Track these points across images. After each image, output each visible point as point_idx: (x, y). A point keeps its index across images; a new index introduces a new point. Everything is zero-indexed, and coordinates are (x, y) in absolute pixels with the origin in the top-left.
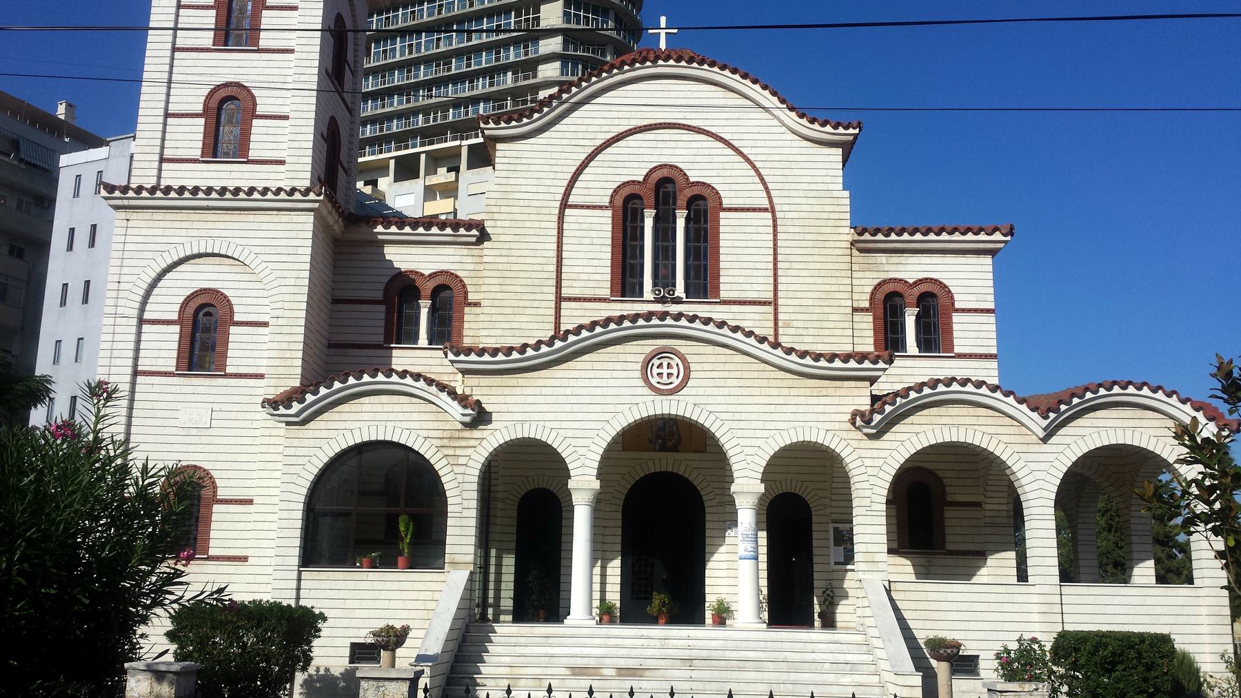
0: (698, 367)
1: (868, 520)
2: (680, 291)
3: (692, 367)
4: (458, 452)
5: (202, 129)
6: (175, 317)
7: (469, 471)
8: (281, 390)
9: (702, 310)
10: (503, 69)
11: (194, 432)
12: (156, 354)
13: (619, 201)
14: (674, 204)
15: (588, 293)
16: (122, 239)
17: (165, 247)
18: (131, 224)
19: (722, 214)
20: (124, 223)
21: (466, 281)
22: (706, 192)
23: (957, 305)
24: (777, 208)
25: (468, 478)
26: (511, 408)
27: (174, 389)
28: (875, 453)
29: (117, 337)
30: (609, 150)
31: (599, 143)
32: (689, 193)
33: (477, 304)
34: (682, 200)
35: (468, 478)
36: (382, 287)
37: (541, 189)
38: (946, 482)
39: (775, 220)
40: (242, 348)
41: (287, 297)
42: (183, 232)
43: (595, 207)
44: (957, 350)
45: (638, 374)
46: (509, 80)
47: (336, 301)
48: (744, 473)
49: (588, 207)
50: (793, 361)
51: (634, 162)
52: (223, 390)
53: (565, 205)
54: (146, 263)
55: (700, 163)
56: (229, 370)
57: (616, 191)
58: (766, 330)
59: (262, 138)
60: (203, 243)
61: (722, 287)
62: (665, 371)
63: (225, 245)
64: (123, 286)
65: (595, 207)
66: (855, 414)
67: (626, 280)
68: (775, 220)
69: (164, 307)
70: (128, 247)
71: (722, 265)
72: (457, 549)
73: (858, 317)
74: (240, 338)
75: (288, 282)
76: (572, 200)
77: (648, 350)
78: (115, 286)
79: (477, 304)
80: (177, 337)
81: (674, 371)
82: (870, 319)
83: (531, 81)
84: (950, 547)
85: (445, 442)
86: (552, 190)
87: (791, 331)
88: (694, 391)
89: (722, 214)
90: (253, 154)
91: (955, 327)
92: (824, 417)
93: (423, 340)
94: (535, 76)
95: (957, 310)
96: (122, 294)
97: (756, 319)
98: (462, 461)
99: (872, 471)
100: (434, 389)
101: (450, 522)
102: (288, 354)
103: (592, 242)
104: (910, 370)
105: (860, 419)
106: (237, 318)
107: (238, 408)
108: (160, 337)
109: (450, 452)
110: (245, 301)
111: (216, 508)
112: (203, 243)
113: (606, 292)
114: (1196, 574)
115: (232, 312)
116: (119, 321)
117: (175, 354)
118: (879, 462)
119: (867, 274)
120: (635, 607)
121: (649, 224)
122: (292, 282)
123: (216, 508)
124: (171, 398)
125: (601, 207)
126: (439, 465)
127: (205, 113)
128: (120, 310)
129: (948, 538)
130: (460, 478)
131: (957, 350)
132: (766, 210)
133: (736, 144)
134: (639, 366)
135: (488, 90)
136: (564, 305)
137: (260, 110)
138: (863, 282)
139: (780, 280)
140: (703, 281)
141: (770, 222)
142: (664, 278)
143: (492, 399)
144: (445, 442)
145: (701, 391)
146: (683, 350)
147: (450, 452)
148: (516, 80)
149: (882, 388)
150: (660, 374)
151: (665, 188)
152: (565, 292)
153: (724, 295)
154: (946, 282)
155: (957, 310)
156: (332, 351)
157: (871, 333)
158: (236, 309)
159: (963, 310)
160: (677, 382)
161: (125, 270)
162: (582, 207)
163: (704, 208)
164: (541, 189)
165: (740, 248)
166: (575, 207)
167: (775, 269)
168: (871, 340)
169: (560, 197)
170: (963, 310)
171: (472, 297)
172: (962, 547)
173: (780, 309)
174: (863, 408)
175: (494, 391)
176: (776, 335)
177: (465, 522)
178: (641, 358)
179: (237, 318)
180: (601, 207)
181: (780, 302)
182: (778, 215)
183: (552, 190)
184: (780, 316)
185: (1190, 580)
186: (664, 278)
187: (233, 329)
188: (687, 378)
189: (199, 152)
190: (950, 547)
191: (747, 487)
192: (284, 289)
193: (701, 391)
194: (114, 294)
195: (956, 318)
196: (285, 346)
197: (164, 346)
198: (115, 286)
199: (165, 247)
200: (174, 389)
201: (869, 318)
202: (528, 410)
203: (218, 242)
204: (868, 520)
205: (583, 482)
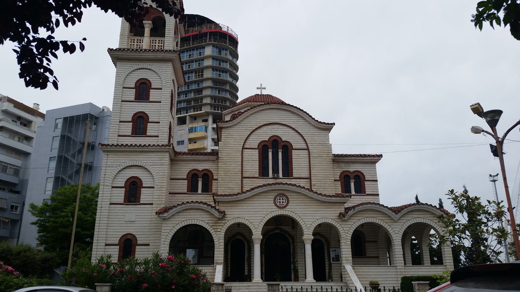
0: (292, 199)
1: (345, 247)
2: (281, 175)
3: (273, 204)
4: (218, 227)
5: (131, 126)
6: (123, 185)
7: (221, 233)
8: (159, 209)
9: (285, 181)
10: (190, 91)
11: (130, 222)
12: (117, 197)
13: (261, 147)
14: (278, 147)
15: (252, 176)
16: (106, 161)
17: (121, 163)
18: (109, 156)
19: (293, 151)
20: (107, 156)
21: (213, 172)
22: (288, 144)
23: (366, 179)
24: (310, 149)
25: (221, 236)
26: (234, 213)
27: (123, 209)
28: (347, 226)
29: (104, 192)
30: (257, 131)
31: (254, 129)
32: (282, 144)
33: (217, 180)
34: (280, 147)
35: (221, 236)
36: (186, 174)
37: (236, 143)
38: (366, 234)
39: (309, 152)
40: (145, 195)
41: (160, 179)
42: (126, 159)
43: (253, 149)
44: (367, 193)
45: (273, 202)
46: (192, 95)
47: (171, 179)
48: (307, 233)
49: (251, 149)
50: (315, 196)
51: (265, 134)
52: (139, 209)
53: (243, 148)
54: (114, 168)
55: (286, 135)
56: (141, 202)
57: (260, 144)
58: (307, 186)
59: (151, 129)
60: (133, 162)
61: (294, 173)
62: (281, 201)
63: (140, 162)
64: (106, 176)
65: (253, 149)
66: (341, 213)
67: (263, 172)
68: (309, 152)
69: (120, 183)
70: (108, 163)
71: (293, 167)
72: (218, 258)
73: (336, 183)
74: (144, 192)
75: (160, 174)
76: (246, 146)
77: (276, 194)
78: (104, 176)
79: (217, 180)
80: (124, 192)
81: (284, 201)
82: (340, 183)
83: (201, 96)
84: (367, 255)
85: (214, 224)
86: (240, 143)
87: (315, 187)
88: (290, 207)
89: (293, 151)
90: (148, 134)
91: (366, 186)
92: (329, 215)
93: (200, 191)
94: (202, 94)
95: (367, 181)
96: (106, 179)
97: (303, 183)
98: (219, 230)
99: (346, 232)
100: (210, 208)
101: (215, 250)
102: (161, 197)
103: (253, 158)
104: (355, 200)
105: (341, 216)
106: (144, 185)
107: (144, 214)
108: (118, 192)
109: (215, 227)
110: (146, 180)
111: (137, 247)
112: (133, 162)
113: (257, 175)
114: (444, 262)
115: (142, 184)
116: (105, 187)
117: (123, 197)
118: (348, 229)
119: (338, 169)
120: (433, 263)
121: (270, 154)
122: (162, 174)
123: (137, 247)
124: (122, 211)
125: (255, 149)
126: (212, 232)
127: (132, 121)
128: (105, 184)
129: (367, 252)
130: (218, 236)
131: (367, 193)
132: (306, 149)
133: (296, 129)
134: (273, 199)
135: (185, 98)
136: (244, 179)
137: (150, 120)
138: (337, 172)
139: (312, 171)
140: (288, 172)
141: (308, 153)
142: (276, 171)
143: (228, 210)
144: (214, 224)
145: (293, 207)
146: (287, 194)
147: (215, 227)
148: (195, 95)
149: (346, 205)
150: (280, 202)
151: (275, 143)
152: (307, 151)
153: (294, 176)
154: (363, 172)
155: (367, 181)
156: (170, 195)
157: (340, 188)
158: (143, 183)
159: (368, 181)
160: (285, 204)
161: (107, 171)
162: (249, 149)
163: (287, 148)
164: (236, 143)
165: (299, 160)
166: (247, 149)
167: (310, 168)
168: (340, 190)
169: (242, 146)
170: (368, 181)
171: (215, 177)
172: (371, 255)
173: (312, 180)
174: (342, 212)
175: (228, 208)
176: (311, 188)
177: (220, 250)
178: (273, 197)
179: (144, 185)
180: (255, 149)
181: (312, 178)
182: (310, 151)
183: (240, 143)
184: (312, 183)
185: (423, 264)
186: (276, 171)
187: (142, 189)
188: (288, 203)
189: (130, 133)
190: (367, 255)
191: (308, 236)
192: (160, 176)
193: (293, 207)
194: (103, 179)
195: (366, 183)
196: (159, 194)
197: (120, 195)
198: (104, 176)
199: (121, 163)
200: (123, 209)
201: (339, 183)
202: (236, 215)
203: (138, 161)
204: (345, 247)
205: (257, 235)
